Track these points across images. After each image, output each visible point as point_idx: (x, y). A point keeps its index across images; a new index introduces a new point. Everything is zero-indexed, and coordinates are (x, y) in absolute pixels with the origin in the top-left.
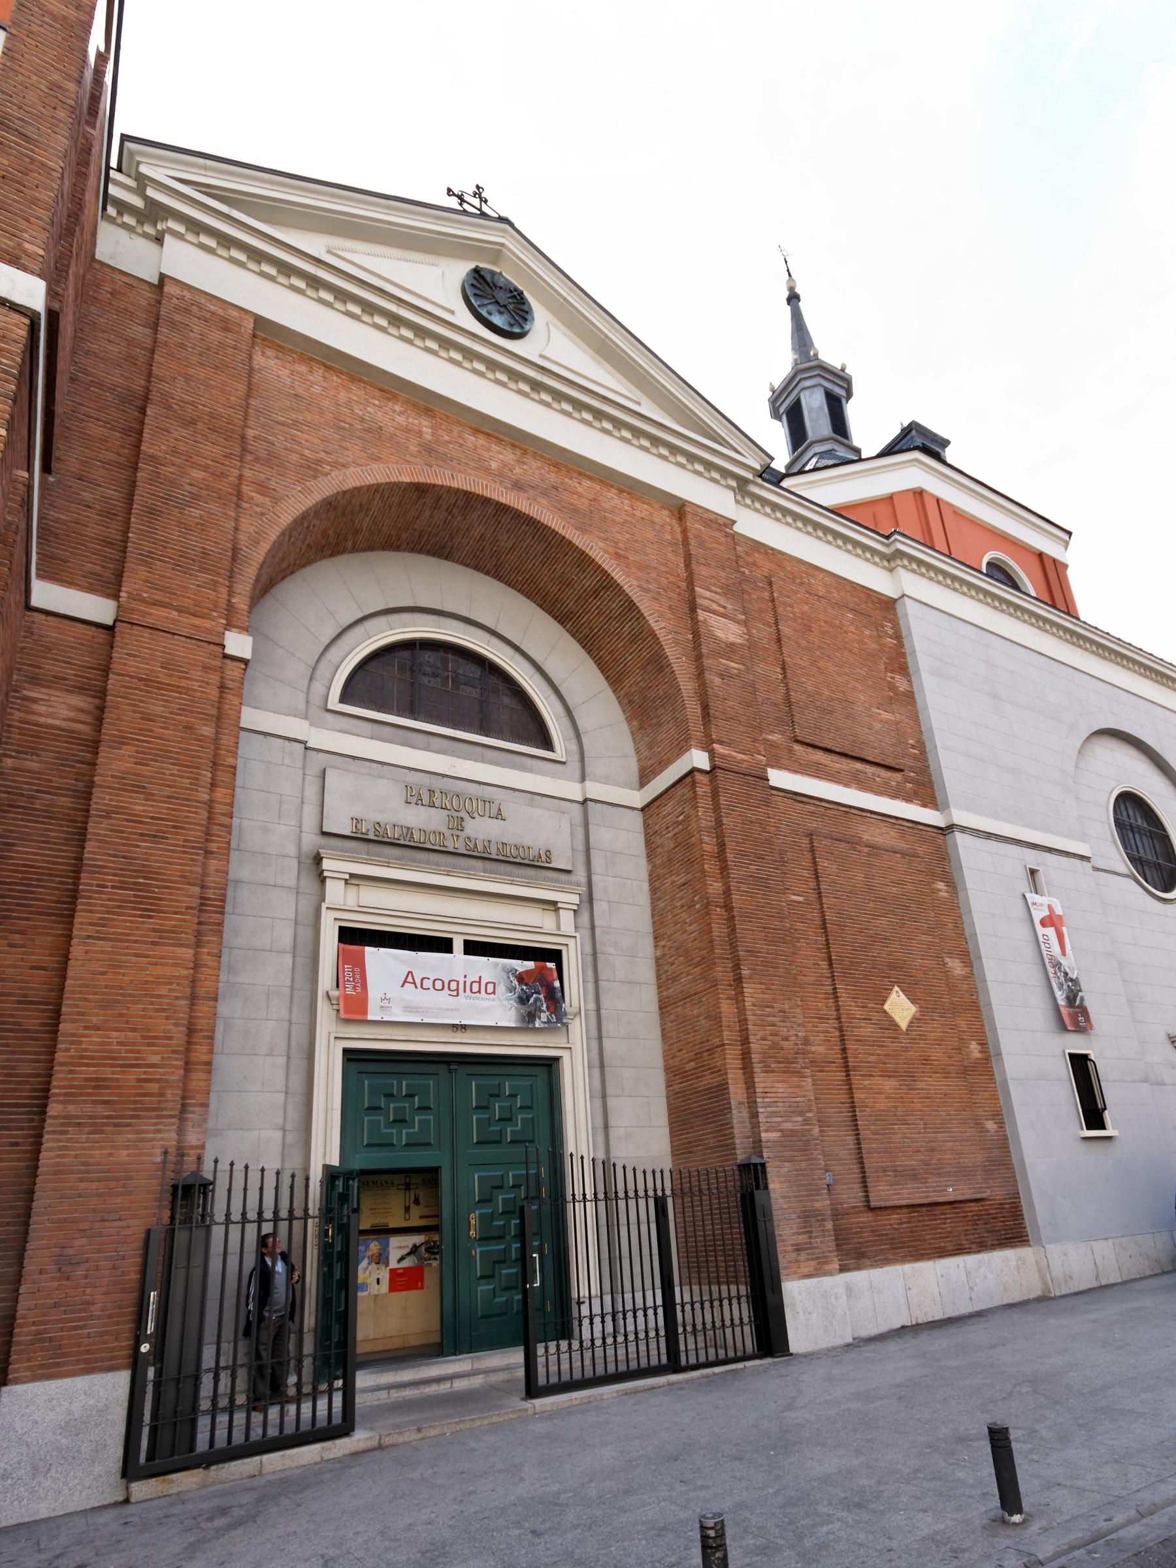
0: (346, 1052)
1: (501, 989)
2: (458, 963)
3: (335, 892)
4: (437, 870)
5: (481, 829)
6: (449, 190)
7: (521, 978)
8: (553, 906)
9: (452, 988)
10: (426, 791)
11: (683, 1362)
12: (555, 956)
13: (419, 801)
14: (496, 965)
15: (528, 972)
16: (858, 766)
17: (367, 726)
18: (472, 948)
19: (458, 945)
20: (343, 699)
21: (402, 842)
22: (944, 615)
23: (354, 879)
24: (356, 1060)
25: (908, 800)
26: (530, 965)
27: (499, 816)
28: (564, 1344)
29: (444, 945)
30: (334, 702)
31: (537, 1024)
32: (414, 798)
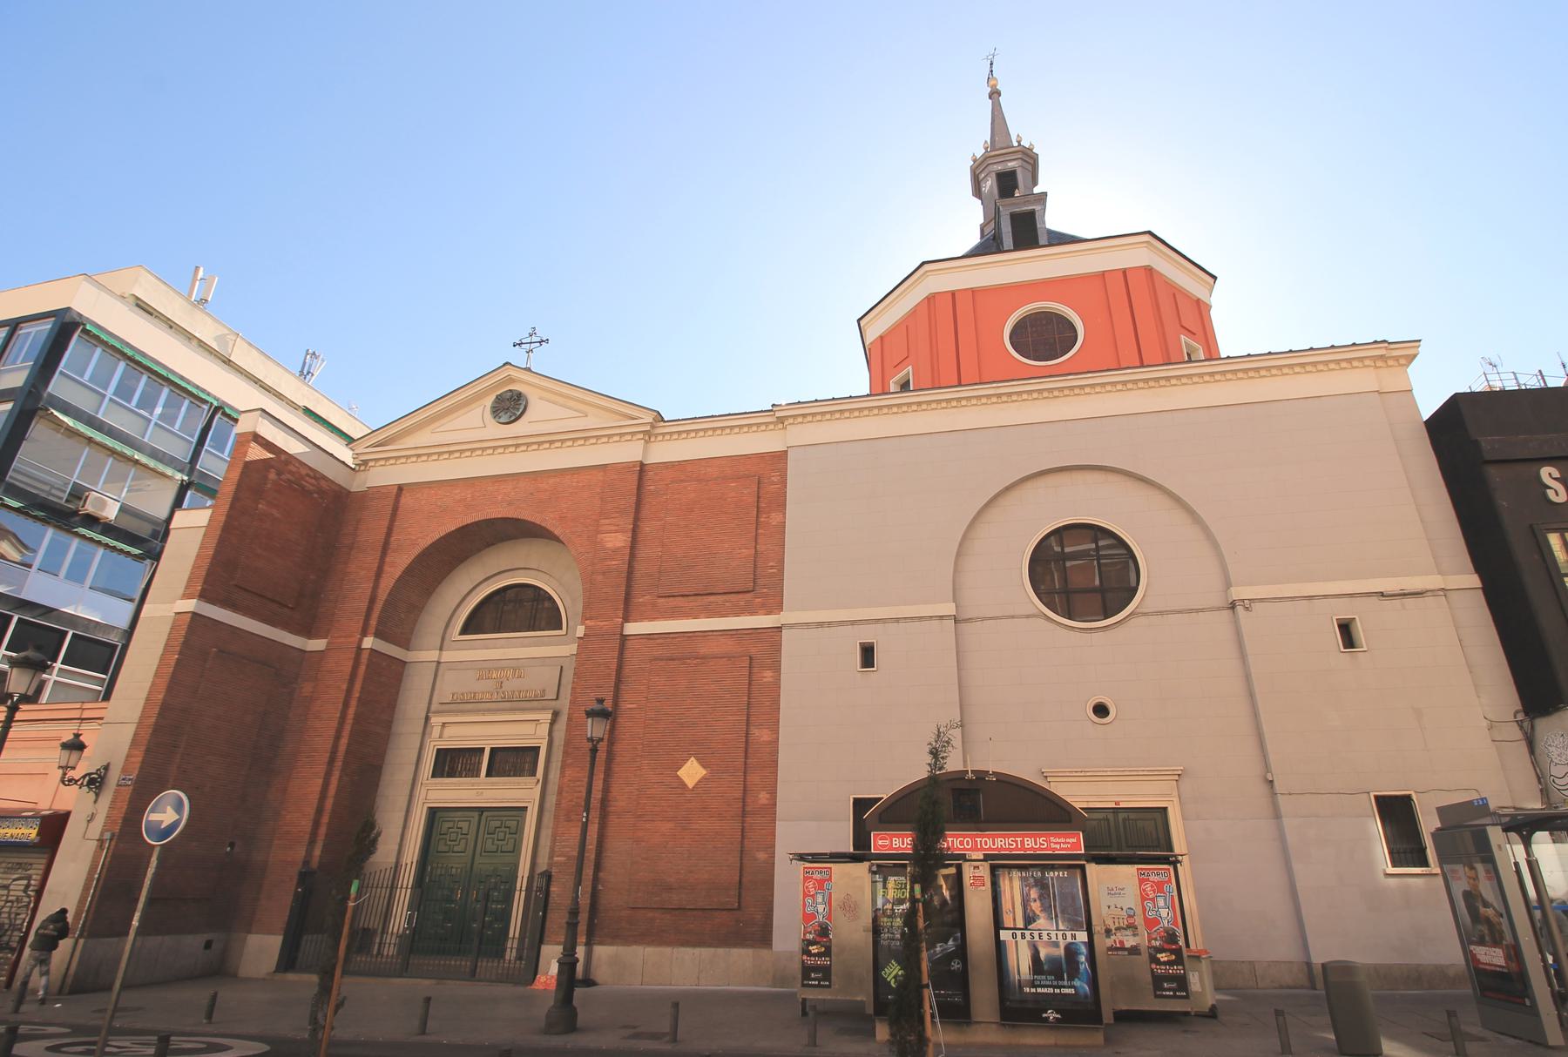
3: (436, 732)
5: (511, 685)
10: (485, 670)
16: (712, 598)
25: (752, 613)
30: (563, 632)
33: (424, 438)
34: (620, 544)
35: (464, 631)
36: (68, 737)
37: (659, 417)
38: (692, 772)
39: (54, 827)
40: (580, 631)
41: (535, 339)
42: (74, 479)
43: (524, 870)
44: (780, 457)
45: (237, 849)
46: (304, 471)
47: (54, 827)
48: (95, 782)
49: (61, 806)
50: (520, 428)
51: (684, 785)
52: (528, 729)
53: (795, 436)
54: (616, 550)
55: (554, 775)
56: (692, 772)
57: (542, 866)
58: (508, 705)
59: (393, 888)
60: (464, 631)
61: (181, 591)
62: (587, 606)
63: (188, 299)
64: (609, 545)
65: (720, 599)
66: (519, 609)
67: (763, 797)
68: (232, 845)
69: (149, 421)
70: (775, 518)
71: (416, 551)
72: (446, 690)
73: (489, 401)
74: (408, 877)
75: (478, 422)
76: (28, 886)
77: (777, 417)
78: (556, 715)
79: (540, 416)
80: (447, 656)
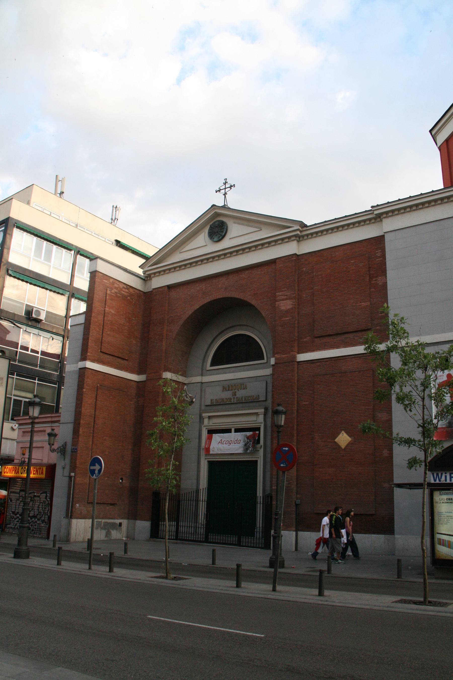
0: (209, 462)
1: (242, 441)
2: (233, 435)
3: (206, 421)
4: (249, 408)
5: (241, 393)
6: (63, 192)
7: (248, 438)
8: (257, 414)
9: (229, 443)
10: (227, 386)
11: (242, 544)
12: (258, 429)
13: (226, 390)
14: (242, 434)
15: (250, 436)
16: (347, 336)
17: (234, 369)
18: (237, 430)
19: (233, 430)
20: (263, 359)
21: (227, 403)
22: (435, 223)
23: (210, 417)
24: (211, 464)
26: (251, 433)
27: (245, 388)
28: (252, 538)
29: (229, 431)
30: (265, 361)
31: (248, 451)
32: (225, 389)
33: (177, 258)
34: (289, 307)
35: (212, 364)
36: (49, 430)
37: (303, 225)
38: (343, 439)
39: (51, 470)
40: (273, 361)
41: (228, 186)
42: (26, 303)
43: (260, 493)
44: (379, 242)
45: (124, 481)
46: (121, 286)
47: (51, 470)
48: (62, 451)
49: (52, 462)
50: (226, 243)
51: (339, 447)
52: (253, 418)
53: (389, 225)
54: (287, 311)
55: (55, 569)
56: (343, 439)
57: (268, 492)
58: (241, 405)
59: (197, 500)
60: (212, 364)
61: (79, 357)
62: (274, 347)
63: (55, 194)
64: (283, 308)
65: (351, 336)
66: (237, 351)
67: (385, 453)
68: (122, 479)
69: (50, 266)
70: (380, 280)
71: (181, 322)
72: (208, 398)
73: (207, 230)
74: (203, 496)
75: (202, 245)
76: (46, 496)
77: (377, 215)
78: (266, 409)
79: (236, 235)
80: (206, 379)
